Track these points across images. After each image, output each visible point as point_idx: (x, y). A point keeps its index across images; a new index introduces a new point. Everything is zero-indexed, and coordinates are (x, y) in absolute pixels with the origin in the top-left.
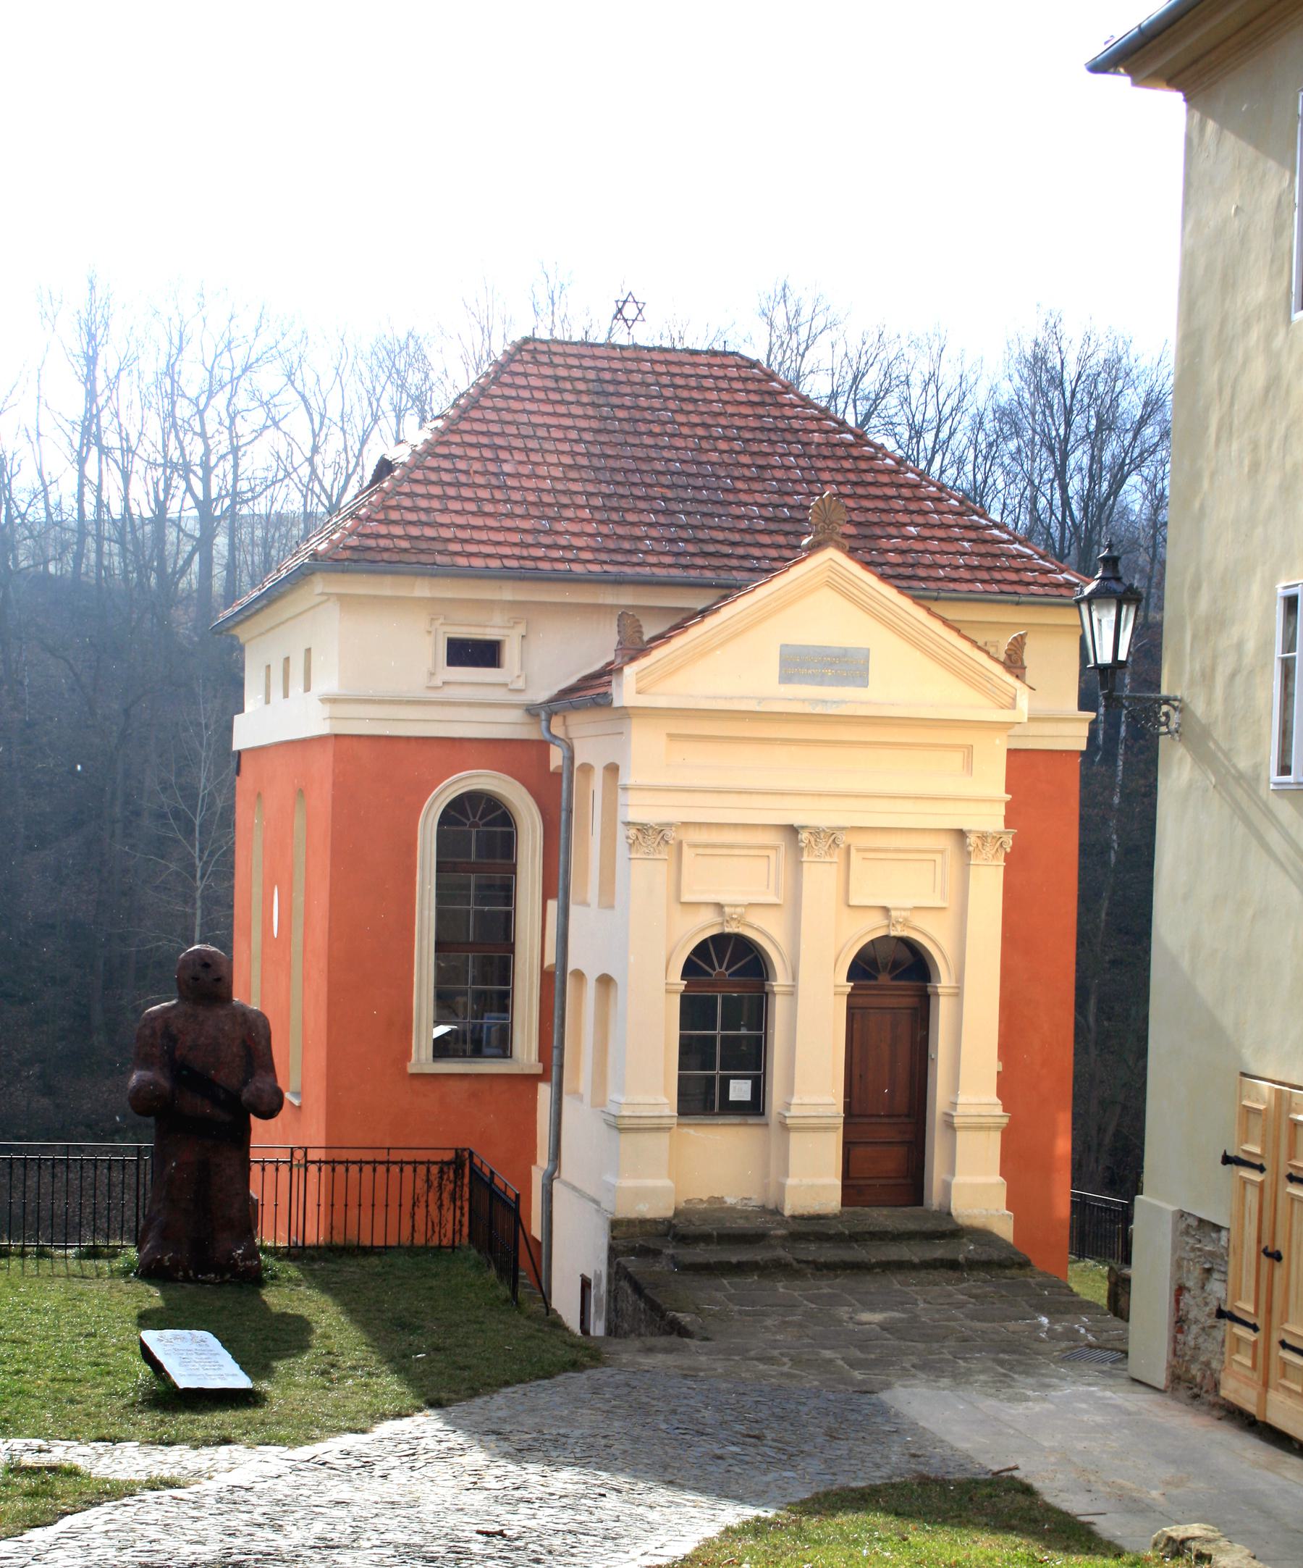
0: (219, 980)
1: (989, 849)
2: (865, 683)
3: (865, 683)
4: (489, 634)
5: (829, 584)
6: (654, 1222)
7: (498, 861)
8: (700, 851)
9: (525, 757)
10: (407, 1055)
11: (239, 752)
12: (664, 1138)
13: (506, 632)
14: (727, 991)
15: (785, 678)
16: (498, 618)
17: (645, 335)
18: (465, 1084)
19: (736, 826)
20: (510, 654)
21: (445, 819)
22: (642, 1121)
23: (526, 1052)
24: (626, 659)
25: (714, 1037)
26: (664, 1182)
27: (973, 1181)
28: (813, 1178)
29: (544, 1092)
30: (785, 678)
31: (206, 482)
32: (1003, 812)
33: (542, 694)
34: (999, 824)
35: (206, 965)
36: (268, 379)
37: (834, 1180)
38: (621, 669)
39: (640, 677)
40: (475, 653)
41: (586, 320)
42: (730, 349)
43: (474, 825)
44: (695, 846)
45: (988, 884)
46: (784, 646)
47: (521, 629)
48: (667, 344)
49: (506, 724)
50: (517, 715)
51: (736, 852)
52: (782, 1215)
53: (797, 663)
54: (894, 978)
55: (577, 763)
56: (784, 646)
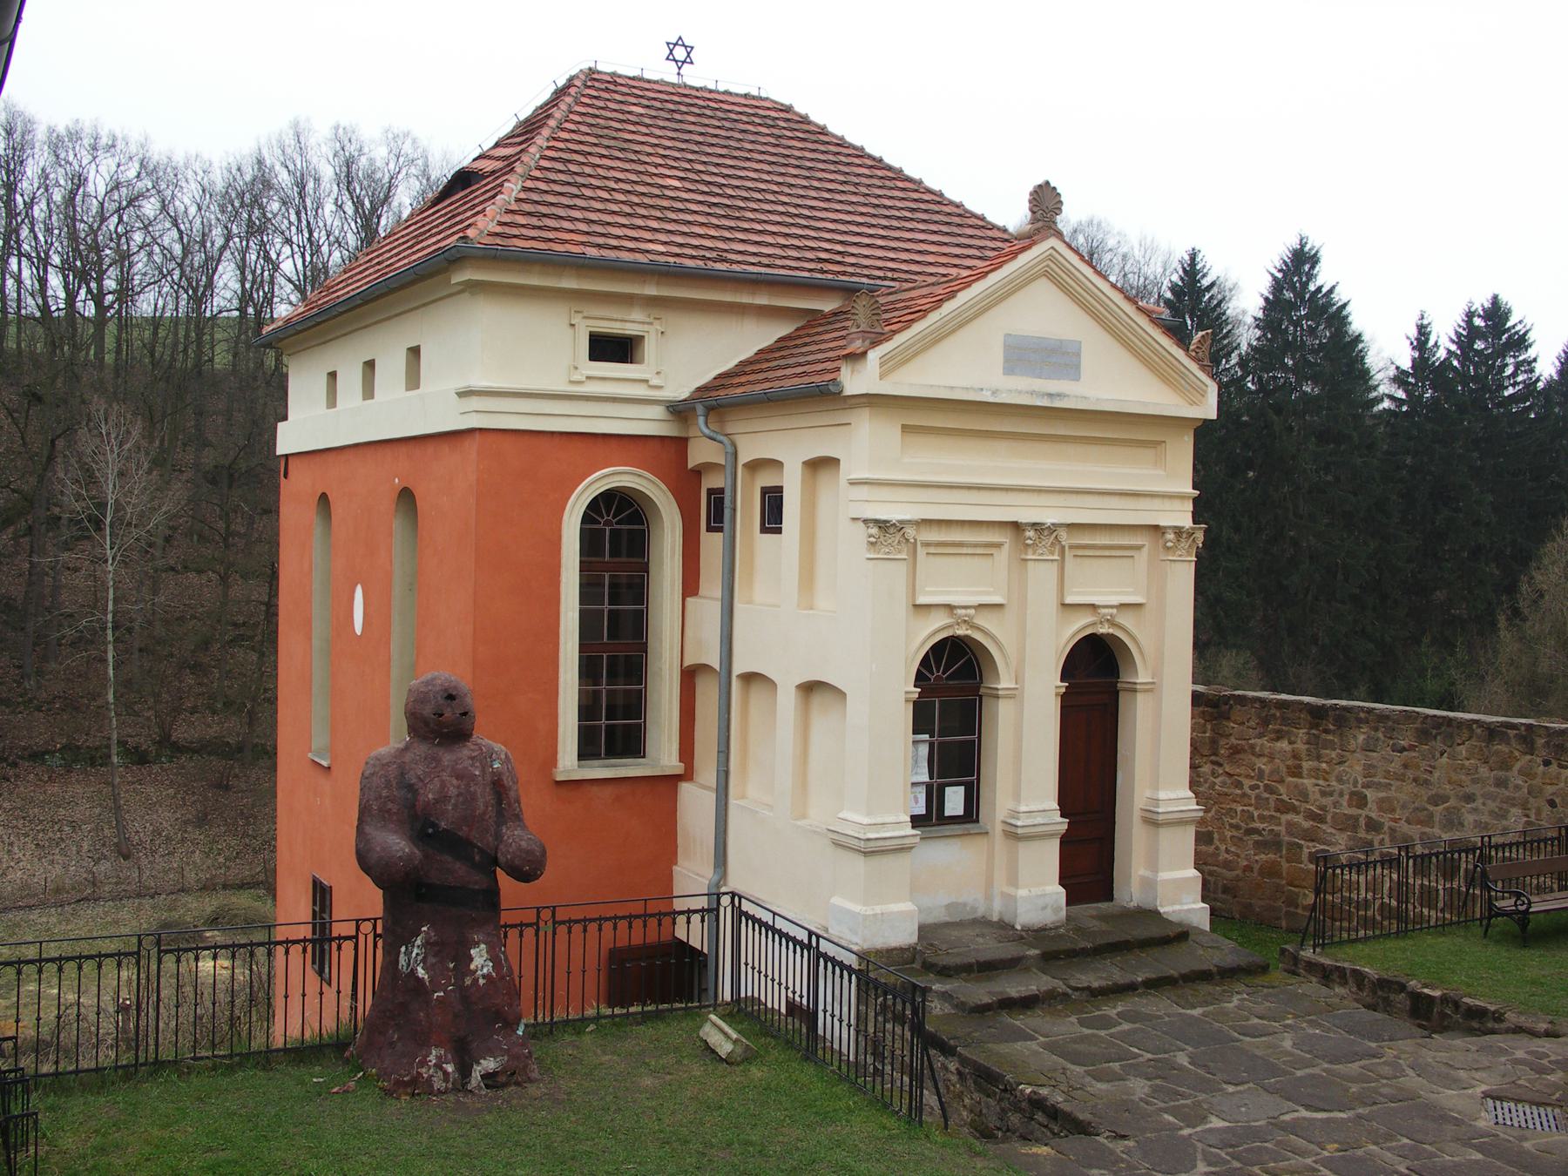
0: (465, 714)
1: (1184, 544)
2: (1077, 378)
3: (1077, 378)
4: (630, 329)
5: (1046, 274)
6: (901, 950)
7: (624, 559)
8: (932, 550)
9: (667, 454)
10: (552, 760)
11: (287, 456)
12: (904, 860)
13: (646, 328)
14: (952, 687)
15: (1009, 369)
16: (637, 314)
17: (695, 77)
18: (608, 792)
19: (940, 523)
20: (650, 348)
21: (586, 519)
22: (888, 843)
23: (663, 754)
24: (867, 343)
25: (608, 691)
26: (907, 906)
27: (1165, 876)
28: (1036, 892)
29: (695, 803)
30: (1009, 369)
31: (100, 280)
32: (1190, 507)
33: (680, 390)
34: (1186, 521)
35: (451, 697)
36: (150, 208)
37: (1056, 893)
38: (864, 353)
39: (884, 361)
40: (613, 348)
41: (638, 57)
42: (763, 95)
43: (607, 523)
44: (927, 544)
45: (1181, 580)
46: (1007, 336)
47: (658, 326)
48: (755, 93)
49: (649, 422)
50: (658, 412)
51: (965, 550)
52: (1013, 927)
53: (1020, 355)
54: (1096, 671)
55: (743, 458)
56: (1007, 336)
